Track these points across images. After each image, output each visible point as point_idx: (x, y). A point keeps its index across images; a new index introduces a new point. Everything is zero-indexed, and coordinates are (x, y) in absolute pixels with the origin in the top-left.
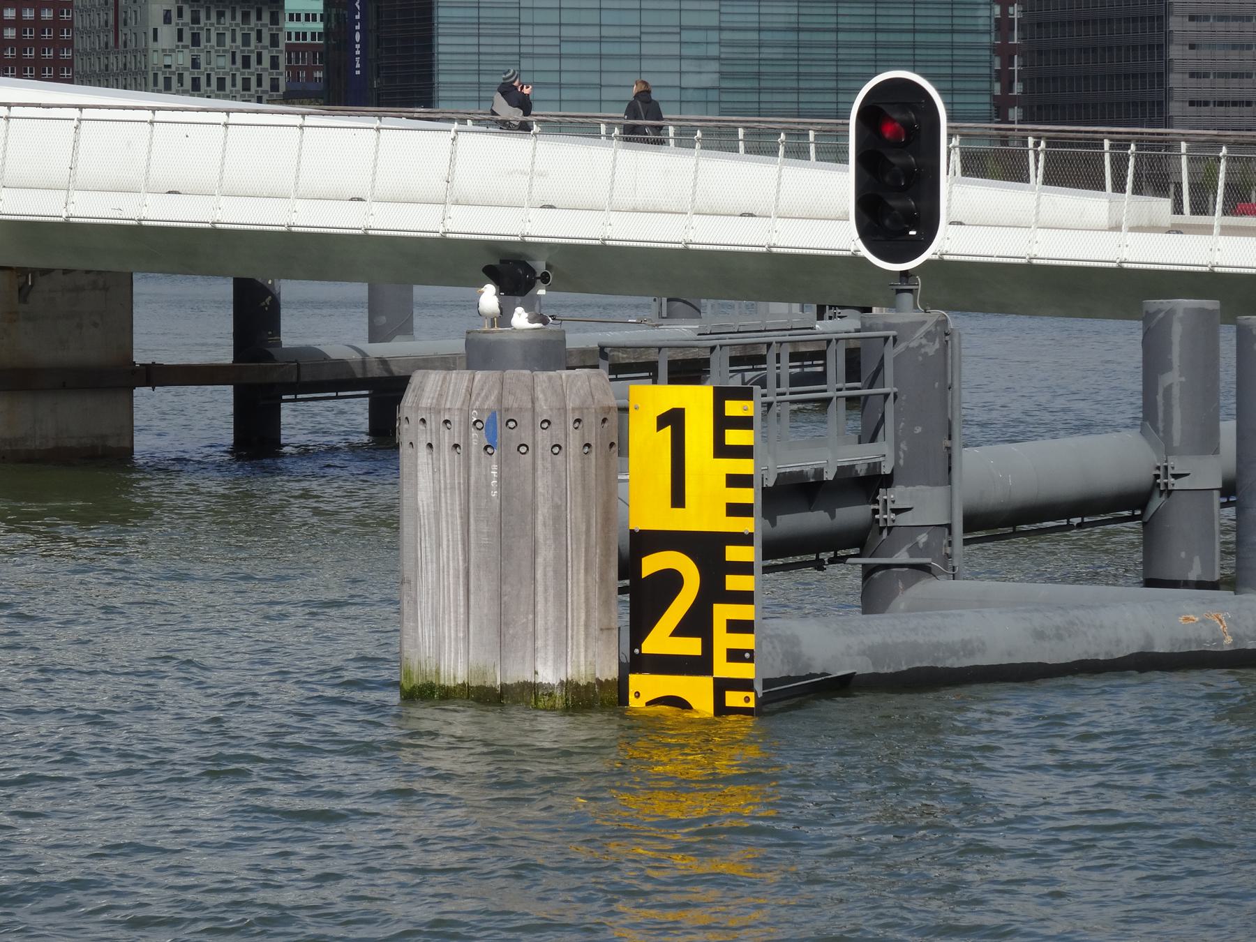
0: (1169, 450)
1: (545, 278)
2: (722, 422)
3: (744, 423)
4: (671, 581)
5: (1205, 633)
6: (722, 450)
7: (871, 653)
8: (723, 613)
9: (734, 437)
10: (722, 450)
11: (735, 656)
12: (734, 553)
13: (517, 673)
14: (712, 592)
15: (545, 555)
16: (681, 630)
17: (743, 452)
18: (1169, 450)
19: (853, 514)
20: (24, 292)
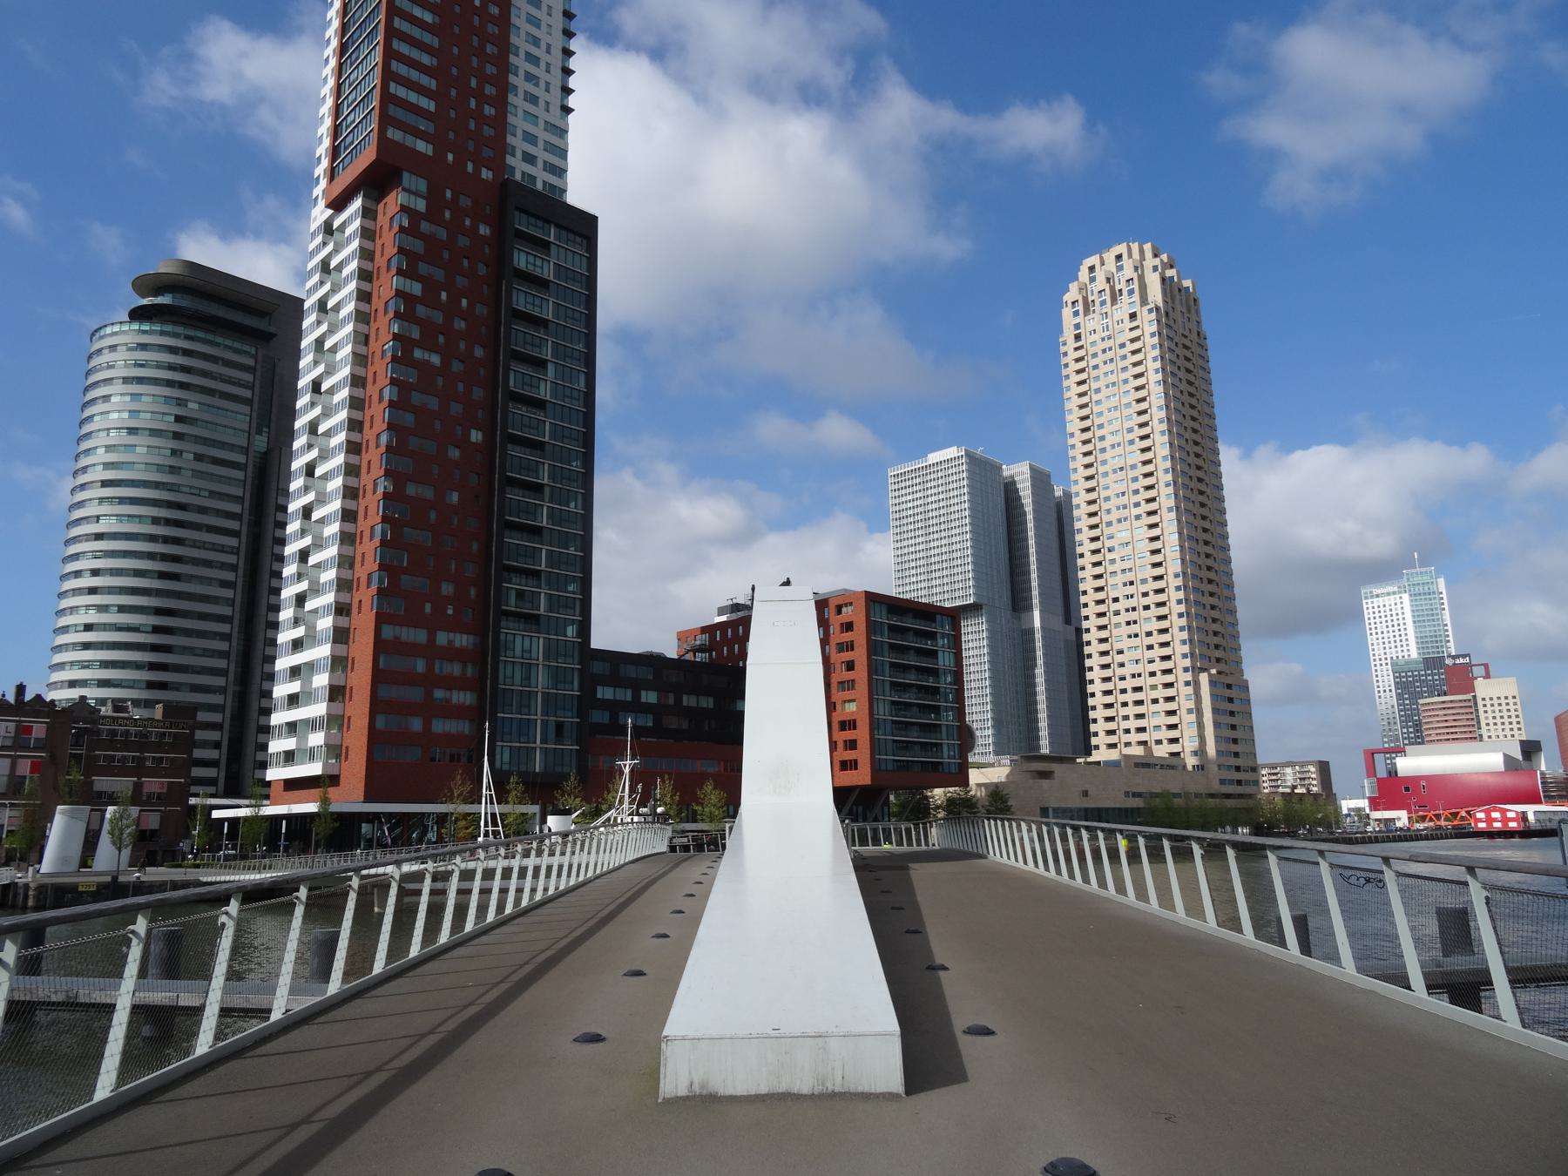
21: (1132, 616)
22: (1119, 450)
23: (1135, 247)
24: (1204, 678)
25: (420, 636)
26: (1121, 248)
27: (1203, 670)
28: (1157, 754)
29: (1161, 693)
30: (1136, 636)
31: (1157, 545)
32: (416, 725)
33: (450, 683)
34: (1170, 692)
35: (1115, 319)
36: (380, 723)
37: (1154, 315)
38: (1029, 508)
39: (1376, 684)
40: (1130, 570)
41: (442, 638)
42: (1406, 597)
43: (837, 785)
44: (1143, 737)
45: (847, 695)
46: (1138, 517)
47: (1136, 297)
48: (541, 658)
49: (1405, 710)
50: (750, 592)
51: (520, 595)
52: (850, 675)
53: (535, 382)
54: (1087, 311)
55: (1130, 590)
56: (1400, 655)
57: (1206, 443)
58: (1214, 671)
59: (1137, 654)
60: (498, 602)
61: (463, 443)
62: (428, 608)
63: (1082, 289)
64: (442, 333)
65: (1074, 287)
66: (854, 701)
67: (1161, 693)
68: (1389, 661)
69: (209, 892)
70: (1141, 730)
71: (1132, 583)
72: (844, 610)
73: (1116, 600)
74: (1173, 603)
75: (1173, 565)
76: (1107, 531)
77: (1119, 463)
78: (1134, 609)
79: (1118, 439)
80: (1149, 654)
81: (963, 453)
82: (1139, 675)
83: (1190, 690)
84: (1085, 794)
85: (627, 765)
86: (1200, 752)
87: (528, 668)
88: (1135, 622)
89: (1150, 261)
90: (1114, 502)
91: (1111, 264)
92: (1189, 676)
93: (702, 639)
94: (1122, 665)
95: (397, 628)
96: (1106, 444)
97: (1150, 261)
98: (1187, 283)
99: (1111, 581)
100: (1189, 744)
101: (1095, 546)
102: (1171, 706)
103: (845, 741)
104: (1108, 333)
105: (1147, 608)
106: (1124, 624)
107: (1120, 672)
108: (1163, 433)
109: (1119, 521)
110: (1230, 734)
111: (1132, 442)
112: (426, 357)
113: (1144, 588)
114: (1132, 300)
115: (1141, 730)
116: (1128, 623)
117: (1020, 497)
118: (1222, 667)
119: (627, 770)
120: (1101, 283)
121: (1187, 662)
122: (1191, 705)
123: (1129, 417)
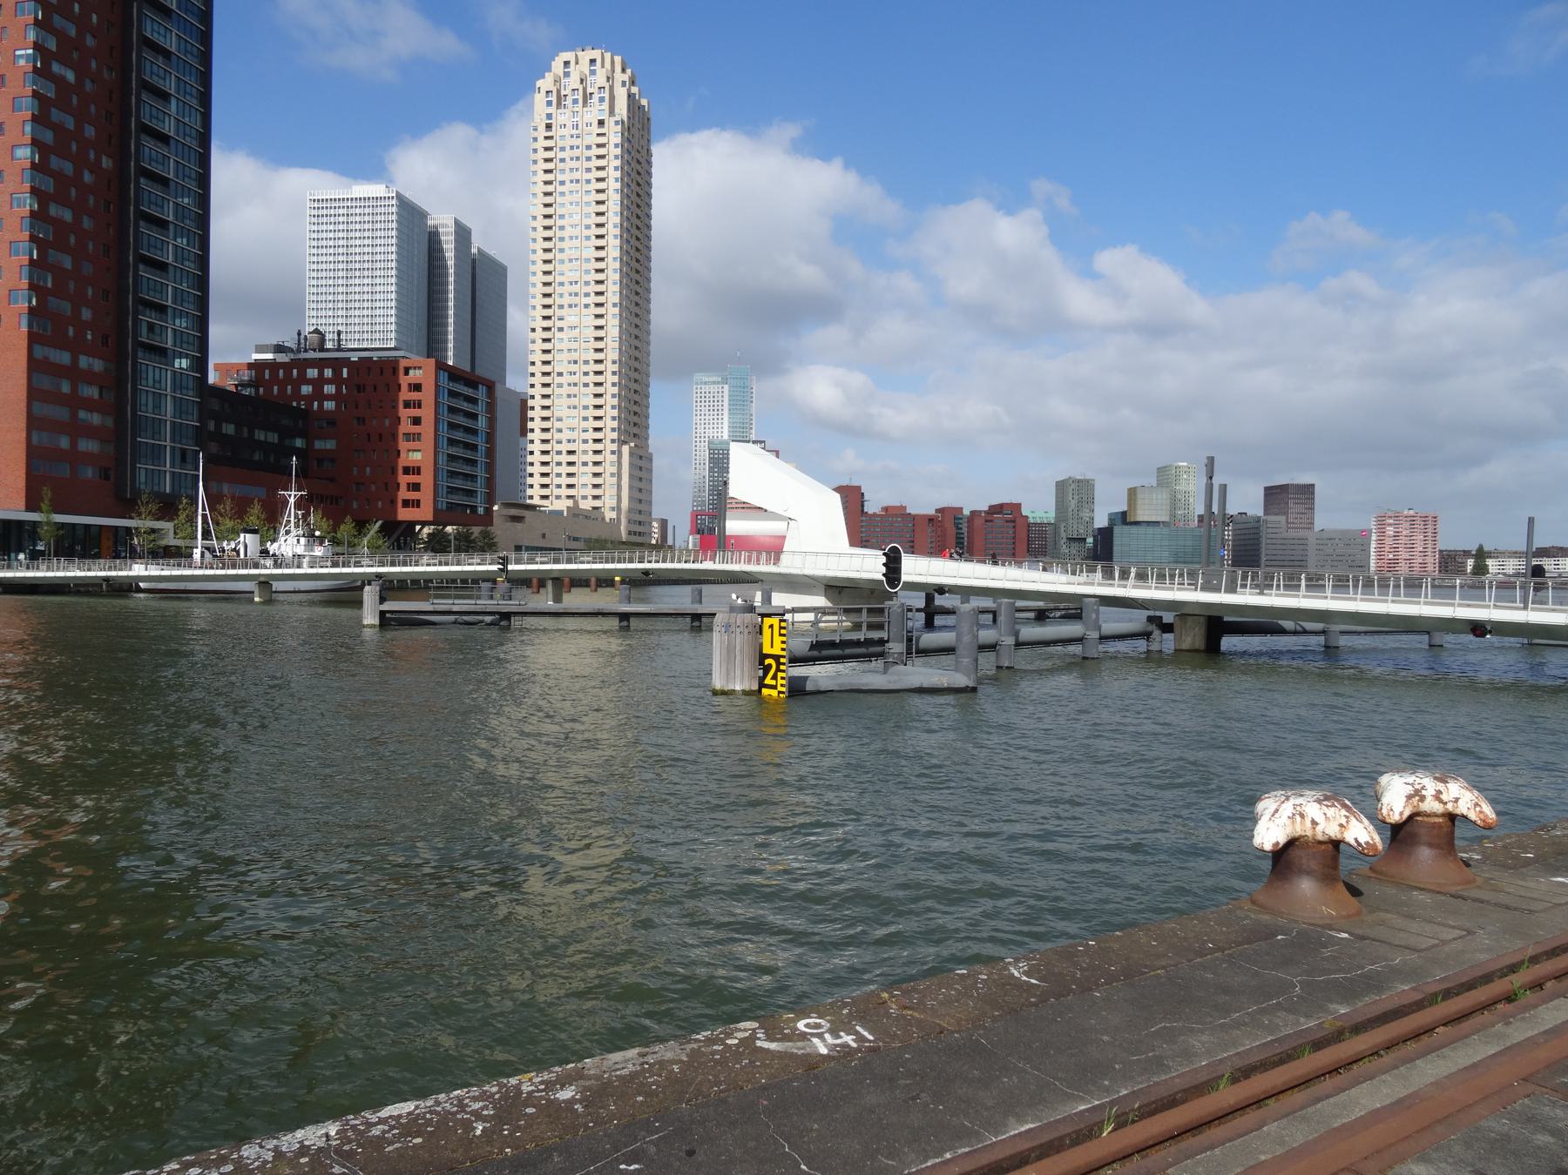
0: (1001, 635)
1: (1490, 632)
2: (781, 628)
3: (784, 628)
4: (770, 666)
5: (939, 683)
6: (781, 635)
7: (838, 685)
8: (780, 675)
9: (783, 631)
10: (781, 635)
11: (782, 685)
12: (782, 660)
13: (731, 687)
14: (778, 670)
15: (738, 658)
16: (772, 678)
17: (784, 635)
18: (1001, 635)
19: (878, 649)
20: (872, 593)
21: (574, 390)
22: (576, 243)
23: (608, 56)
24: (625, 449)
25: (64, 358)
26: (596, 54)
27: (625, 442)
28: (581, 506)
29: (591, 458)
30: (575, 407)
31: (600, 333)
32: (64, 443)
33: (90, 405)
34: (598, 458)
35: (585, 121)
36: (35, 439)
37: (619, 128)
38: (451, 263)
39: (694, 457)
40: (575, 350)
41: (84, 362)
42: (726, 387)
43: (24, 508)
44: (571, 492)
45: (411, 445)
46: (586, 306)
47: (606, 106)
48: (169, 390)
49: (713, 481)
50: (297, 337)
51: (151, 327)
52: (416, 429)
53: (161, 116)
54: (559, 105)
55: (574, 368)
56: (716, 435)
57: (644, 251)
58: (632, 445)
59: (574, 423)
60: (136, 333)
61: (95, 168)
62: (71, 331)
63: (557, 81)
64: (77, 49)
65: (549, 77)
66: (419, 451)
67: (591, 458)
68: (707, 439)
69: (45, 577)
70: (570, 486)
71: (575, 362)
72: (411, 372)
73: (560, 374)
74: (609, 385)
75: (612, 353)
76: (559, 313)
77: (574, 254)
78: (575, 385)
79: (576, 232)
80: (584, 424)
81: (394, 195)
82: (574, 441)
83: (614, 458)
84: (544, 536)
85: (292, 496)
86: (618, 508)
87: (158, 398)
88: (575, 396)
89: (620, 77)
90: (567, 288)
91: (584, 66)
92: (614, 447)
93: (246, 376)
94: (560, 431)
95: (91, 359)
96: (565, 234)
97: (620, 77)
98: (644, 102)
99: (558, 357)
100: (608, 501)
101: (546, 324)
102: (598, 469)
103: (408, 484)
104: (577, 132)
105: (586, 385)
106: (565, 396)
107: (557, 436)
108: (616, 237)
109: (570, 306)
110: (639, 496)
111: (588, 238)
112: (63, 72)
113: (585, 368)
114: (602, 107)
115: (570, 486)
116: (569, 396)
117: (442, 249)
118: (638, 443)
119: (292, 500)
120: (573, 81)
121: (615, 435)
122: (614, 470)
123: (588, 215)
